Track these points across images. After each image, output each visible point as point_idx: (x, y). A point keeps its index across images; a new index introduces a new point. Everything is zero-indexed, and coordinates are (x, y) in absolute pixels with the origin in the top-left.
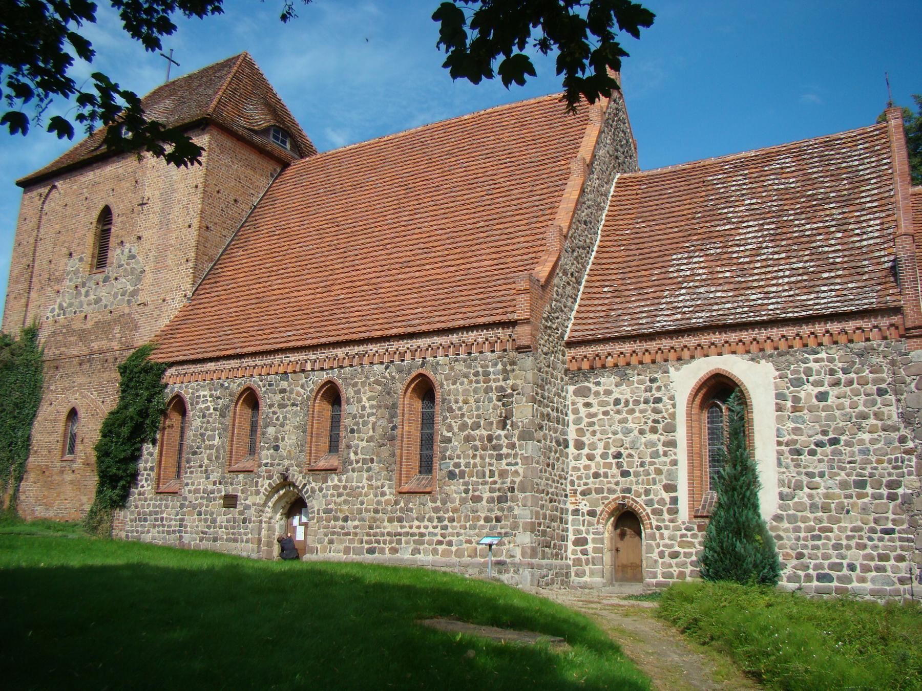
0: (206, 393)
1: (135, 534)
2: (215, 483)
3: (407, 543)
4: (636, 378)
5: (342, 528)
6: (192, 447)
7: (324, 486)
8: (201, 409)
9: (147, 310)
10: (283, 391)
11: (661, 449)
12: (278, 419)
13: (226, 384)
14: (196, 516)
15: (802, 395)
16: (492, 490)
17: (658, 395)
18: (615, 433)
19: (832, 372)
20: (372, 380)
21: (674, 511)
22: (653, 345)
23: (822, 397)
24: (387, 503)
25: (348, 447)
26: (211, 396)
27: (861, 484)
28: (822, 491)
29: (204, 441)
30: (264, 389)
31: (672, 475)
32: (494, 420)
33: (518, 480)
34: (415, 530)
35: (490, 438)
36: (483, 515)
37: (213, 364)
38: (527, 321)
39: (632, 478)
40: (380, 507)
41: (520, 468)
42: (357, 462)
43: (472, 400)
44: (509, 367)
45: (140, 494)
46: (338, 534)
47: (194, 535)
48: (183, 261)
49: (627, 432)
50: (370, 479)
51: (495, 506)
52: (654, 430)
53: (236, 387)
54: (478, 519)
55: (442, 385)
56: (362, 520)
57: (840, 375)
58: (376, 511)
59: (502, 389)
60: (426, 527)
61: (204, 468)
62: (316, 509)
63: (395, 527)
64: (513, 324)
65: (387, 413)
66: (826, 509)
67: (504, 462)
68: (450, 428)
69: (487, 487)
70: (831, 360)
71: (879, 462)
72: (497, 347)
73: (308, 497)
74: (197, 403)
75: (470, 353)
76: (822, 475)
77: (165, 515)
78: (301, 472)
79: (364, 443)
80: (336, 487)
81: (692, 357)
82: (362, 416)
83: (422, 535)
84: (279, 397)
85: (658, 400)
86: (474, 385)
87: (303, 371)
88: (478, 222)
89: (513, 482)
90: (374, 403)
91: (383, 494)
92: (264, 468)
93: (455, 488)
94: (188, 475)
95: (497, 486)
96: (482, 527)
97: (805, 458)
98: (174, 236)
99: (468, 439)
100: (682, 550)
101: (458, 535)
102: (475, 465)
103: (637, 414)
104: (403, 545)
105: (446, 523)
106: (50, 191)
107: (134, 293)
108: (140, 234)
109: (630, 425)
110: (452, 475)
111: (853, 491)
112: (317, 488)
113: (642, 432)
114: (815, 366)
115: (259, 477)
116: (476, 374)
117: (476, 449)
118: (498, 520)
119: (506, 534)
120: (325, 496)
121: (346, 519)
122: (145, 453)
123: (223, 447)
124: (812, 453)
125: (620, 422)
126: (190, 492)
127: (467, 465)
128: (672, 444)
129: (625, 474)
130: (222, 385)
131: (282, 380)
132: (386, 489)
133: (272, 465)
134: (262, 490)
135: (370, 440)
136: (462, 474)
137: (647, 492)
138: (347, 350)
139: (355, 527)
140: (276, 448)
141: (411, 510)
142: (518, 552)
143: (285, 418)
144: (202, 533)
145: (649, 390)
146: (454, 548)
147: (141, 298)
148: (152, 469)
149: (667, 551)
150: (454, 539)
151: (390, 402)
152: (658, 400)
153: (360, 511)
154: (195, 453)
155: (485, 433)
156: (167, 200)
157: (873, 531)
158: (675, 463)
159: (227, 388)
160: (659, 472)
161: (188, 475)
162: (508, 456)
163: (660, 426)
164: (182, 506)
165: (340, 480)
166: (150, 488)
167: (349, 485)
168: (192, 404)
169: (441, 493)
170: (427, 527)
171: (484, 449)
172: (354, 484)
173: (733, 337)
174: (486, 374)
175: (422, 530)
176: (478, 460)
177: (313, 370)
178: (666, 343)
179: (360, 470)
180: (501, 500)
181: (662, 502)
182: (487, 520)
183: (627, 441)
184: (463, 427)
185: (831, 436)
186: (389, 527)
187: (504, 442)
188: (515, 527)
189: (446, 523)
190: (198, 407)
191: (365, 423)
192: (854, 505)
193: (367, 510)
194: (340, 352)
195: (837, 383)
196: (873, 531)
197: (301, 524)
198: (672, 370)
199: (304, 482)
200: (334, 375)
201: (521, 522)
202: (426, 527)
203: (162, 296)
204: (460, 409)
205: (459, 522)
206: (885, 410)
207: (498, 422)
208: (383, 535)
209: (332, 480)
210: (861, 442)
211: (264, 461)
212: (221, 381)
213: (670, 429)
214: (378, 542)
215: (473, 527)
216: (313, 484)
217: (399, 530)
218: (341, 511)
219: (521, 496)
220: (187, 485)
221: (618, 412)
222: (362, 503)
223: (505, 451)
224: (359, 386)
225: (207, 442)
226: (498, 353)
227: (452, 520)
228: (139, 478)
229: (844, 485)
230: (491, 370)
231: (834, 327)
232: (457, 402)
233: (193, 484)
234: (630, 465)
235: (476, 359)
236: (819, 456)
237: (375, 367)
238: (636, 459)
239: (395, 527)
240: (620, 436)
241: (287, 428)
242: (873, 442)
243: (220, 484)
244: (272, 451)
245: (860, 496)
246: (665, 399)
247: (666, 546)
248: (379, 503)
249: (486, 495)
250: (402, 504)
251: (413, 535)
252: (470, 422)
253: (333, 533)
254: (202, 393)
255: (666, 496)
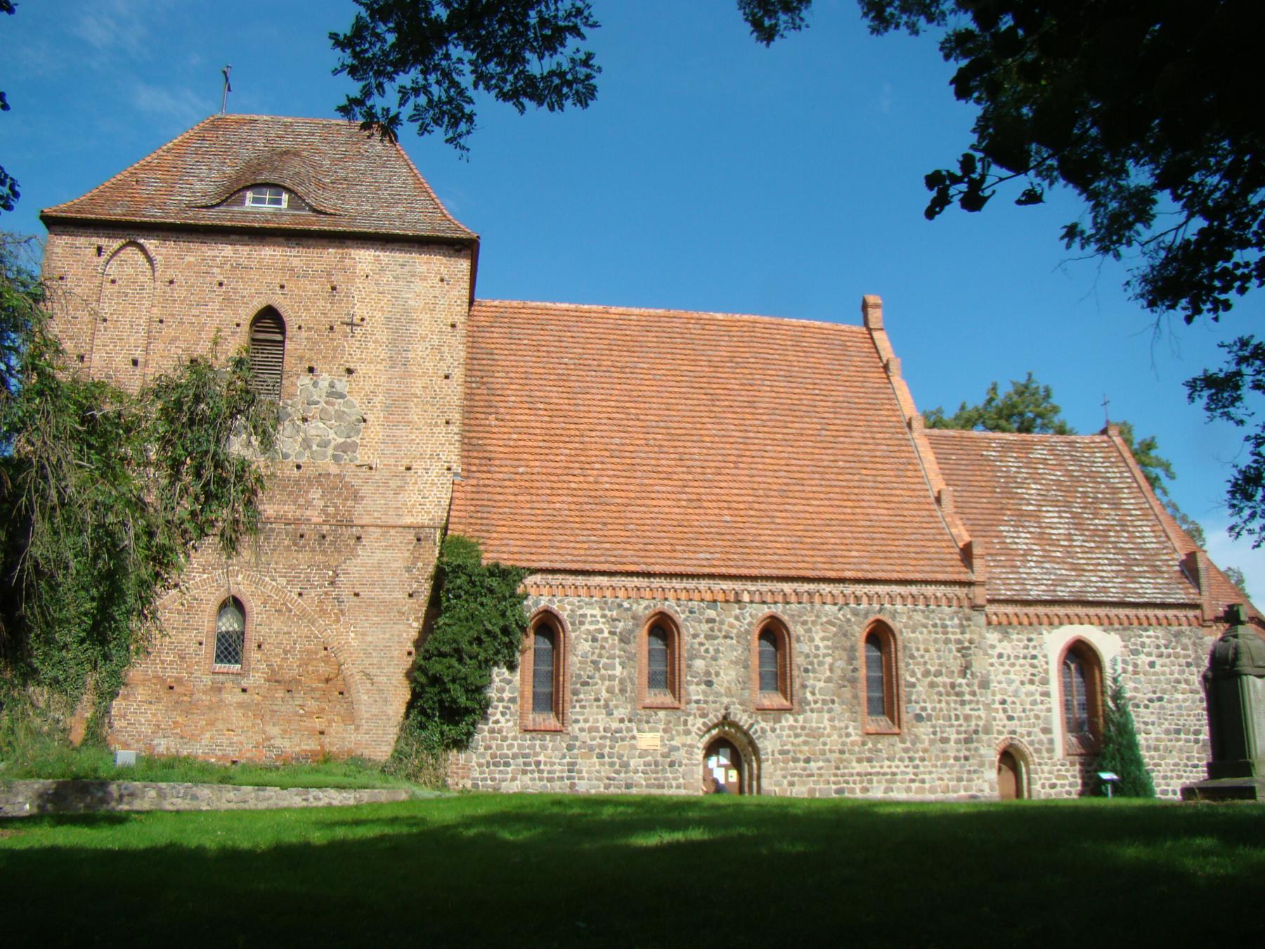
0: (594, 612)
1: (489, 782)
2: (622, 721)
3: (878, 782)
4: (1015, 637)
5: (804, 769)
6: (579, 676)
7: (777, 726)
8: (589, 632)
9: (376, 475)
10: (710, 621)
11: (1039, 698)
12: (707, 651)
13: (626, 605)
14: (595, 759)
15: (1139, 662)
16: (958, 733)
17: (1034, 652)
18: (1000, 683)
19: (1158, 647)
20: (824, 619)
21: (1051, 750)
22: (1031, 610)
23: (1152, 664)
24: (853, 744)
25: (804, 686)
26: (604, 616)
27: (1178, 732)
28: (1153, 735)
29: (599, 670)
30: (683, 616)
31: (1048, 720)
32: (956, 669)
33: (981, 723)
34: (886, 770)
35: (953, 686)
36: (952, 755)
37: (606, 578)
38: (983, 584)
39: (1016, 722)
40: (846, 748)
41: (982, 713)
42: (816, 702)
43: (932, 650)
44: (965, 623)
45: (492, 731)
46: (800, 776)
47: (594, 782)
48: (442, 421)
49: (1010, 682)
50: (831, 720)
51: (963, 746)
52: (1032, 682)
53: (644, 608)
54: (948, 757)
55: (901, 632)
56: (828, 761)
57: (1163, 649)
58: (842, 752)
59: (959, 641)
60: (897, 767)
61: (602, 702)
62: (769, 751)
63: (866, 767)
64: (970, 584)
65: (844, 655)
66: (1156, 749)
67: (967, 707)
68: (913, 674)
69: (954, 729)
70: (1157, 638)
71: (1189, 715)
72: (955, 602)
73: (759, 738)
74: (582, 623)
75: (928, 606)
76: (1153, 724)
77: (541, 758)
78: (744, 711)
79: (822, 684)
80: (791, 728)
81: (1061, 624)
82: (816, 656)
83: (894, 774)
84: (705, 627)
85: (1034, 657)
86: (934, 636)
87: (738, 601)
88: (602, 400)
89: (977, 725)
90: (829, 643)
91: (848, 735)
92: (694, 705)
93: (923, 730)
94: (578, 709)
95: (963, 729)
96: (953, 765)
97: (1142, 710)
98: (420, 383)
99: (932, 685)
100: (1058, 782)
101: (930, 773)
102: (941, 710)
103: (1017, 668)
104: (875, 784)
105: (917, 762)
106: (121, 248)
107: (344, 448)
108: (314, 364)
109: (1012, 676)
110: (919, 718)
111: (1173, 736)
112: (768, 728)
113: (1022, 683)
114: (1147, 641)
115: (689, 714)
116: (935, 625)
117: (940, 694)
118: (966, 758)
119: (975, 772)
120: (778, 737)
121: (807, 761)
122: (497, 679)
123: (631, 680)
124: (1146, 707)
125: (1004, 673)
126: (582, 730)
127: (934, 709)
128: (1046, 694)
129: (1010, 718)
130: (620, 606)
131: (708, 608)
132: (850, 730)
133: (706, 702)
134: (694, 729)
135: (828, 680)
136: (929, 718)
137: (1029, 734)
138: (795, 585)
139: (820, 768)
140: (709, 684)
141: (880, 751)
142: (986, 787)
143: (717, 651)
144: (609, 778)
145: (1026, 647)
146: (927, 786)
147: (361, 456)
148: (512, 700)
149: (1047, 783)
150: (926, 777)
151: (848, 644)
152: (1034, 657)
153: (823, 753)
154: (585, 684)
155: (948, 681)
156: (400, 326)
157: (1186, 765)
158: (1049, 710)
159: (628, 609)
160: (1037, 717)
161: (578, 709)
162: (971, 702)
163: (1036, 679)
164: (570, 748)
165: (796, 721)
166: (511, 724)
167: (808, 725)
168: (573, 624)
169: (909, 734)
170: (899, 767)
171: (948, 694)
172: (814, 725)
173: (1092, 611)
174: (944, 626)
175: (894, 769)
176: (943, 705)
177: (752, 602)
178: (1041, 610)
179: (820, 711)
180: (967, 741)
181: (1041, 742)
182: (957, 759)
183: (1011, 689)
184: (926, 673)
185: (1158, 695)
186: (858, 768)
187: (966, 689)
188: (982, 764)
189: (917, 762)
190: (583, 628)
191: (821, 664)
192: (1174, 747)
193: (831, 751)
194: (787, 587)
195: (1160, 656)
196: (1186, 765)
197: (719, 766)
198: (1045, 632)
199: (750, 721)
200: (778, 610)
201: (987, 760)
202: (897, 767)
203: (406, 462)
204: (922, 656)
205: (930, 760)
206: (1191, 677)
207: (960, 672)
208: (852, 775)
209: (787, 720)
210: (1177, 700)
211: (694, 698)
212: (618, 600)
213: (1045, 682)
214: (847, 782)
215: (944, 766)
216: (763, 724)
217: (870, 770)
218: (801, 752)
219: (985, 737)
220: (577, 721)
221: (1002, 664)
222: (825, 744)
223: (967, 697)
224: (810, 625)
225: (603, 671)
226: (954, 609)
227: (923, 759)
228: (490, 711)
229: (1167, 732)
230: (948, 623)
231: (1160, 613)
232: (918, 650)
233: (586, 721)
234: (1014, 710)
235: (933, 611)
236: (1151, 710)
237: (827, 607)
238: (1018, 705)
239: (866, 767)
240: (1004, 685)
241: (721, 662)
242: (1185, 700)
243: (630, 721)
244: (703, 687)
245: (1178, 740)
246: (1040, 657)
247: (1046, 779)
248: (844, 744)
249: (953, 737)
250: (870, 745)
251: (884, 774)
252: (932, 669)
253: (793, 775)
254: (589, 612)
255: (1044, 737)
